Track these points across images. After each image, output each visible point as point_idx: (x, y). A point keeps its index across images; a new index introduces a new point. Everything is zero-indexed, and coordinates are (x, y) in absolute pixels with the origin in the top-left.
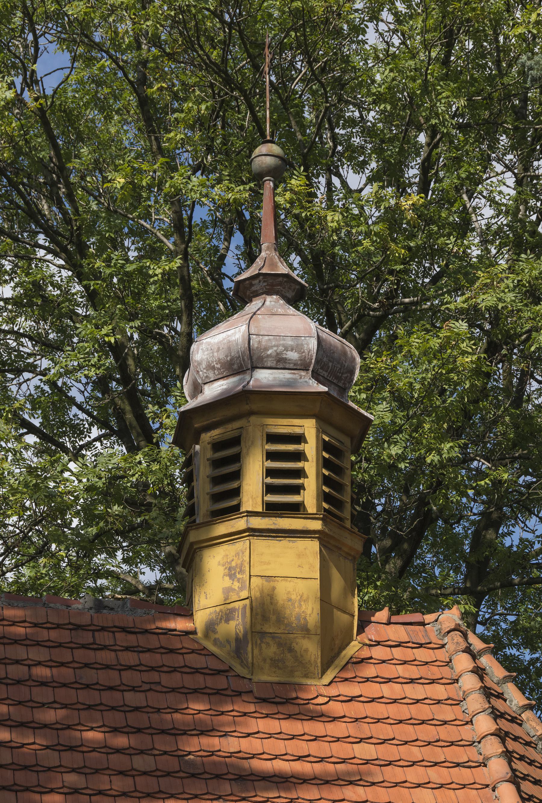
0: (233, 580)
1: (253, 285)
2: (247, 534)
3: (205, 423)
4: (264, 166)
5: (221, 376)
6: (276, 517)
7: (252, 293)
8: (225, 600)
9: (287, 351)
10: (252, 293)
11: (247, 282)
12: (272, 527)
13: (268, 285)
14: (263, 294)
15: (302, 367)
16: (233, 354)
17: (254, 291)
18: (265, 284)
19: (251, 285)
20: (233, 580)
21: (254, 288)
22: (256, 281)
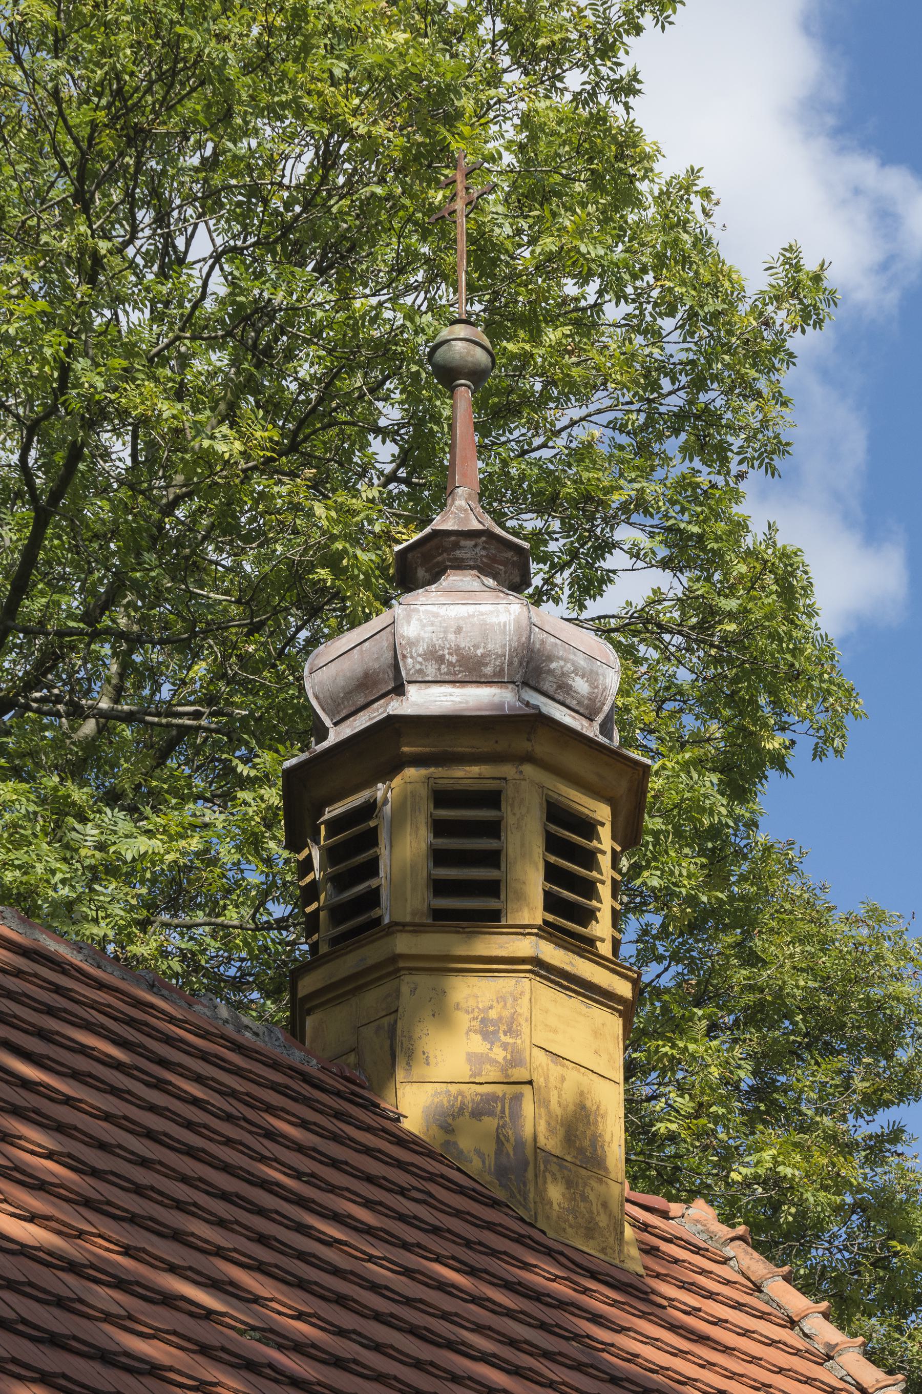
0: (492, 1044)
1: (460, 548)
2: (529, 967)
3: (428, 750)
4: (470, 359)
5: (451, 678)
6: (574, 952)
7: (450, 560)
8: (474, 1075)
9: (576, 675)
10: (450, 560)
11: (453, 538)
12: (568, 968)
13: (487, 556)
14: (471, 568)
15: (586, 712)
16: (490, 646)
17: (456, 559)
18: (484, 553)
19: (456, 546)
20: (492, 1044)
21: (458, 554)
22: (470, 543)
